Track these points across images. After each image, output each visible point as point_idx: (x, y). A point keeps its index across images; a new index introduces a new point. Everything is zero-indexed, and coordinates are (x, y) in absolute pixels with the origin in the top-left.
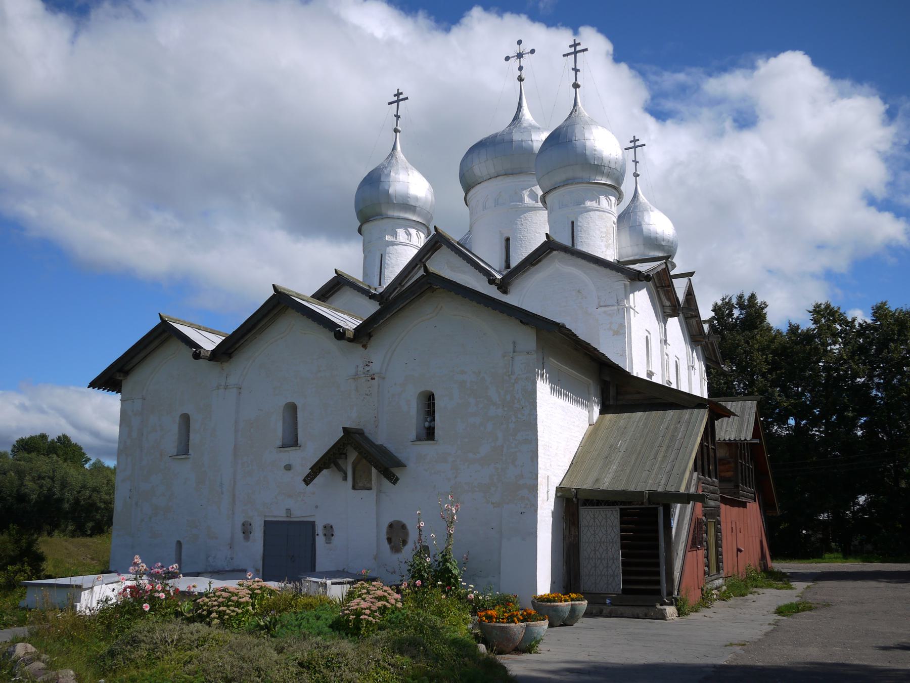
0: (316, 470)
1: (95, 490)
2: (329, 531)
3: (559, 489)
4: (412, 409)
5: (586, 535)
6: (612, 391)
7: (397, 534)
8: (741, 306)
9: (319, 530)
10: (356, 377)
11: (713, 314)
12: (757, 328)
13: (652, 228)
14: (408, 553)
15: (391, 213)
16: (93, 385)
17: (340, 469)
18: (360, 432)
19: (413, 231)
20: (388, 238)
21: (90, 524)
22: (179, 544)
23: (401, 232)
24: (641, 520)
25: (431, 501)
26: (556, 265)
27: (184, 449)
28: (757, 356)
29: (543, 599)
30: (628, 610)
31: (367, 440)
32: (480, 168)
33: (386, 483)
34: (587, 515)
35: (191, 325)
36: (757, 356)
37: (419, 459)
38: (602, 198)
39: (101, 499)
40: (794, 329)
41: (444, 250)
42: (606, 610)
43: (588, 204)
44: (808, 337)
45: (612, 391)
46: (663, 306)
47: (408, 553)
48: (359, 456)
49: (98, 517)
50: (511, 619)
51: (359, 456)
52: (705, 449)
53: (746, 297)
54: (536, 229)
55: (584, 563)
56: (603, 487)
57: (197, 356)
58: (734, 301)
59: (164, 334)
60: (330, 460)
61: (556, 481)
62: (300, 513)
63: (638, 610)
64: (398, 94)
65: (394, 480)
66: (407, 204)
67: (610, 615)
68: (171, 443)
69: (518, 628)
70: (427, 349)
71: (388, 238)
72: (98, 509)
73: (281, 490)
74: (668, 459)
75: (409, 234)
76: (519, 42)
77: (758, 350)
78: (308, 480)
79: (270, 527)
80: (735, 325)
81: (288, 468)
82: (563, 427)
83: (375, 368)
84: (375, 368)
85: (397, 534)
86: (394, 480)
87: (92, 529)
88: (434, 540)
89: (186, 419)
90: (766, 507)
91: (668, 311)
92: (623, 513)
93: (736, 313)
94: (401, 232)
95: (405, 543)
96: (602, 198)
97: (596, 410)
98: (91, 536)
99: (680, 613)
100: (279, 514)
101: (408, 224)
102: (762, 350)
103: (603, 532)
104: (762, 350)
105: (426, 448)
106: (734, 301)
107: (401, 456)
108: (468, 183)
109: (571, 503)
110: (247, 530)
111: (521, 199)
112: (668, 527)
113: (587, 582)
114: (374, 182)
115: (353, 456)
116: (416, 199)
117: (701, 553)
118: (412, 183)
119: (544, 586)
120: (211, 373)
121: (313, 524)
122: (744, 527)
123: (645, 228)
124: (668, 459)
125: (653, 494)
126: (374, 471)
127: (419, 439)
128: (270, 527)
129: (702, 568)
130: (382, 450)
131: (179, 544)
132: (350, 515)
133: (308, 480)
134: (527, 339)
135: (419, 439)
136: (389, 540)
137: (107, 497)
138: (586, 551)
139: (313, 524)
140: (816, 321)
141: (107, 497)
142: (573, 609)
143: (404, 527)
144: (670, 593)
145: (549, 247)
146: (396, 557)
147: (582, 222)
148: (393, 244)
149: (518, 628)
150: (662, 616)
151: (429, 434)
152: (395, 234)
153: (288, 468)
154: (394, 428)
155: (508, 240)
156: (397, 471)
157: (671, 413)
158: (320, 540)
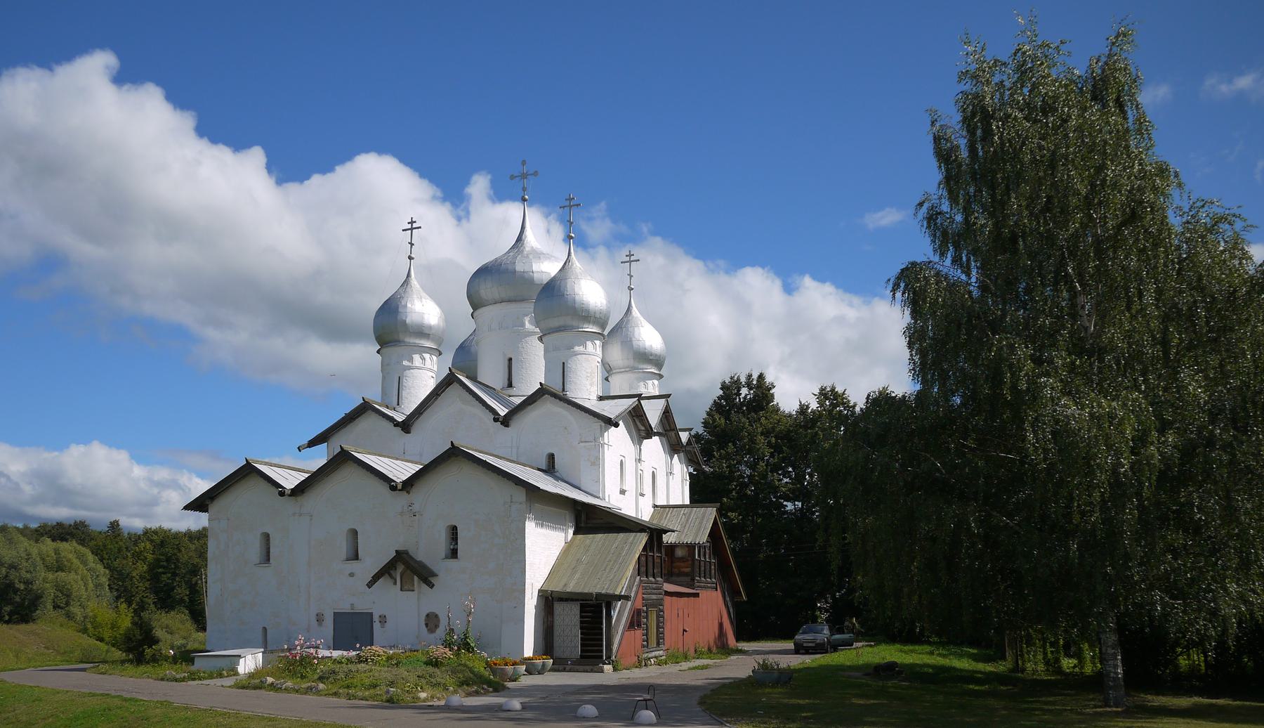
0: (376, 578)
1: (13, 567)
2: (383, 620)
3: (540, 591)
4: (443, 537)
5: (558, 621)
6: (583, 517)
7: (432, 621)
8: (749, 385)
9: (376, 618)
10: (402, 514)
11: (721, 392)
12: (762, 409)
13: (641, 344)
14: (441, 632)
15: (407, 340)
16: (186, 508)
17: (390, 575)
18: (406, 552)
19: (427, 356)
20: (405, 363)
21: (8, 608)
22: (265, 629)
23: (416, 357)
24: (593, 610)
25: (455, 596)
26: (547, 407)
27: (267, 558)
28: (760, 439)
29: (529, 659)
30: (581, 668)
31: (411, 557)
32: (488, 290)
33: (425, 587)
34: (559, 608)
35: (266, 464)
36: (760, 439)
37: (446, 571)
38: (589, 344)
39: (20, 577)
40: (803, 409)
41: (455, 385)
42: (568, 668)
43: (577, 348)
44: (817, 416)
45: (583, 517)
46: (638, 430)
47: (441, 632)
48: (406, 568)
49: (18, 599)
50: (506, 664)
51: (406, 568)
52: (650, 559)
53: (755, 376)
54: (533, 376)
55: (556, 638)
56: (568, 590)
57: (282, 494)
58: (743, 380)
59: (248, 471)
60: (386, 571)
61: (538, 586)
62: (361, 607)
63: (588, 668)
64: (412, 222)
65: (431, 586)
66: (422, 332)
67: (570, 671)
68: (255, 552)
69: (510, 668)
70: (452, 497)
71: (405, 363)
72: (16, 591)
73: (350, 590)
74: (617, 569)
75: (423, 359)
76: (524, 163)
77: (762, 434)
78: (370, 585)
79: (338, 616)
80: (742, 404)
81: (352, 575)
82: (544, 548)
83: (416, 508)
84: (416, 508)
85: (432, 621)
86: (431, 586)
87: (11, 614)
88: (459, 625)
89: (267, 537)
90: (730, 591)
91: (643, 434)
92: (582, 606)
93: (744, 391)
94: (416, 357)
95: (437, 626)
96: (589, 344)
97: (571, 532)
98: (7, 622)
99: (615, 669)
100: (345, 607)
101: (422, 350)
102: (766, 433)
103: (569, 618)
104: (766, 433)
105: (452, 563)
106: (743, 380)
107: (435, 569)
108: (476, 303)
109: (549, 600)
110: (320, 619)
111: (523, 325)
112: (609, 617)
113: (558, 652)
114: (390, 312)
115: (400, 568)
116: (430, 327)
117: (639, 633)
118: (424, 309)
119: (528, 651)
120: (289, 504)
121: (371, 614)
122: (708, 608)
123: (634, 343)
124: (617, 569)
125: (599, 595)
126: (416, 578)
127: (447, 557)
128: (338, 616)
129: (639, 643)
130: (422, 566)
131: (265, 629)
132: (399, 609)
133: (370, 585)
134: (520, 495)
135: (447, 557)
136: (427, 625)
137: (28, 576)
138: (557, 631)
139: (371, 614)
140: (821, 404)
141: (28, 576)
142: (544, 664)
143: (436, 616)
144: (609, 657)
145: (542, 392)
146: (432, 636)
147: (571, 364)
148: (410, 368)
149: (510, 668)
150: (602, 671)
151: (454, 554)
152: (411, 360)
153: (352, 575)
154: (429, 550)
155: (510, 360)
156: (433, 580)
157: (622, 535)
158: (377, 625)
